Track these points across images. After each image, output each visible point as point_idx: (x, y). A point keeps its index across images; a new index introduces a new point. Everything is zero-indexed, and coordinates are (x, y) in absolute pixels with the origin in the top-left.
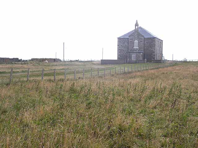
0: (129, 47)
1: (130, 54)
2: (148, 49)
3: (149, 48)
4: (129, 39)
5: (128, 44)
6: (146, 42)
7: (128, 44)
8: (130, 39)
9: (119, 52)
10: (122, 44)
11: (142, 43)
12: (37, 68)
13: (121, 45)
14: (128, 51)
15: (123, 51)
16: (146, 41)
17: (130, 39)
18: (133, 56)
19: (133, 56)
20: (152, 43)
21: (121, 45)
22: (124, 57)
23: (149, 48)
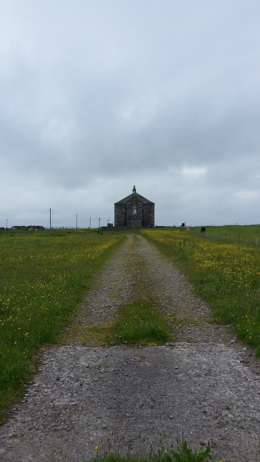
1: (130, 220)
3: (147, 214)
4: (127, 205)
5: (126, 210)
6: (144, 208)
8: (128, 205)
11: (140, 209)
15: (121, 217)
17: (128, 205)
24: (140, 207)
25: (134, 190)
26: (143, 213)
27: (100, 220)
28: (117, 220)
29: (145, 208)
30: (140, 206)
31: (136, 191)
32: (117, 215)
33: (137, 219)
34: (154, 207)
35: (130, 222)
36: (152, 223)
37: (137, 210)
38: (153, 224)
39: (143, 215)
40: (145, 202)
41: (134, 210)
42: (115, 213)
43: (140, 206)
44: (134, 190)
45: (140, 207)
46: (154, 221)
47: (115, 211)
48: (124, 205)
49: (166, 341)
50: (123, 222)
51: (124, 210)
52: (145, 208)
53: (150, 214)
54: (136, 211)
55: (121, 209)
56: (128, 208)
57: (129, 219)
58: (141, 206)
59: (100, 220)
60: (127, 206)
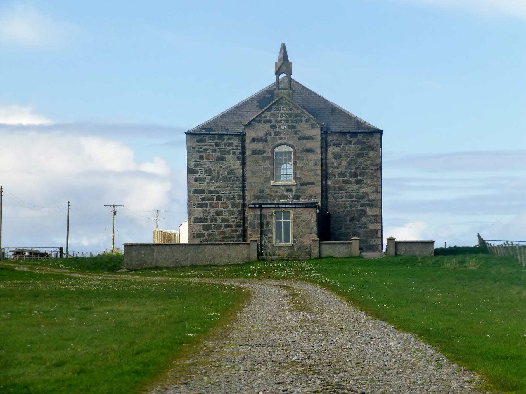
0: (248, 181)
1: (265, 211)
2: (347, 186)
3: (345, 182)
4: (248, 141)
5: (243, 164)
6: (330, 156)
7: (243, 164)
8: (253, 140)
9: (200, 206)
10: (209, 165)
11: (311, 156)
12: (210, 142)
13: (208, 172)
14: (243, 197)
15: (219, 198)
16: (331, 150)
17: (253, 140)
18: (279, 225)
19: (279, 225)
20: (361, 160)
21: (208, 172)
22: (223, 229)
23: (345, 182)
24: (310, 151)
25: (479, 236)
26: (325, 176)
27: (115, 213)
28: (199, 213)
29: (337, 156)
30: (309, 144)
31: (289, 72)
32: (199, 186)
33: (295, 206)
34: (377, 148)
35: (264, 222)
36: (371, 226)
37: (295, 164)
38: (377, 233)
39: (325, 189)
40: (335, 127)
41: (281, 165)
42: (193, 177)
43: (309, 144)
44: (479, 236)
45: (310, 151)
46: (378, 219)
47: (190, 171)
48: (236, 142)
49: (191, 168)
50: (228, 221)
51: (237, 166)
52: (337, 156)
53: (358, 182)
54: (291, 171)
55: (221, 159)
56: (254, 152)
57: (261, 206)
58: (316, 145)
59: (115, 213)
60: (250, 147)
